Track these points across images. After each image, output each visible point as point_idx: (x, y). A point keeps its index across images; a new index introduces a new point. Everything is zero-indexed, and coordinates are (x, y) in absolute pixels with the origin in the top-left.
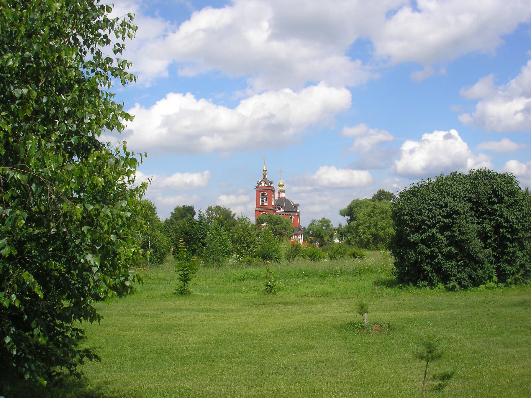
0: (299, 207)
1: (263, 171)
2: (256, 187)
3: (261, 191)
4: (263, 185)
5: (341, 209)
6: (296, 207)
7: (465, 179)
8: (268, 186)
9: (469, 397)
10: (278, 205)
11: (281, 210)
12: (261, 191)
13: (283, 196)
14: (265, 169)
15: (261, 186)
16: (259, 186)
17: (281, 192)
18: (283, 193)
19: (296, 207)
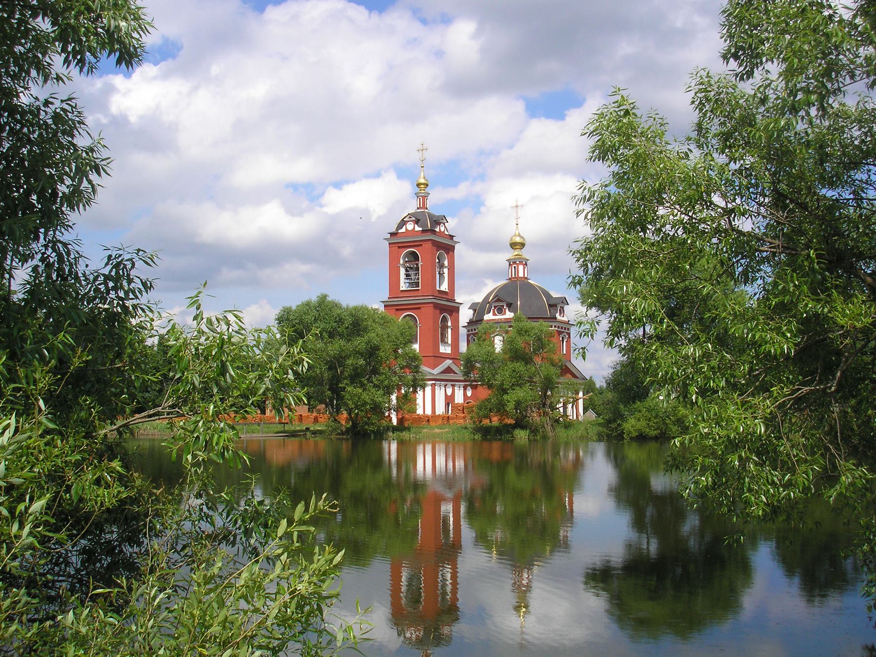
0: (566, 307)
1: (418, 185)
2: (392, 234)
3: (402, 246)
4: (410, 226)
5: (333, 296)
6: (555, 306)
7: (865, 305)
8: (423, 231)
9: (874, 247)
10: (499, 300)
11: (505, 314)
12: (402, 246)
13: (521, 275)
14: (422, 181)
15: (403, 230)
16: (400, 231)
17: (515, 263)
18: (521, 268)
19: (555, 306)
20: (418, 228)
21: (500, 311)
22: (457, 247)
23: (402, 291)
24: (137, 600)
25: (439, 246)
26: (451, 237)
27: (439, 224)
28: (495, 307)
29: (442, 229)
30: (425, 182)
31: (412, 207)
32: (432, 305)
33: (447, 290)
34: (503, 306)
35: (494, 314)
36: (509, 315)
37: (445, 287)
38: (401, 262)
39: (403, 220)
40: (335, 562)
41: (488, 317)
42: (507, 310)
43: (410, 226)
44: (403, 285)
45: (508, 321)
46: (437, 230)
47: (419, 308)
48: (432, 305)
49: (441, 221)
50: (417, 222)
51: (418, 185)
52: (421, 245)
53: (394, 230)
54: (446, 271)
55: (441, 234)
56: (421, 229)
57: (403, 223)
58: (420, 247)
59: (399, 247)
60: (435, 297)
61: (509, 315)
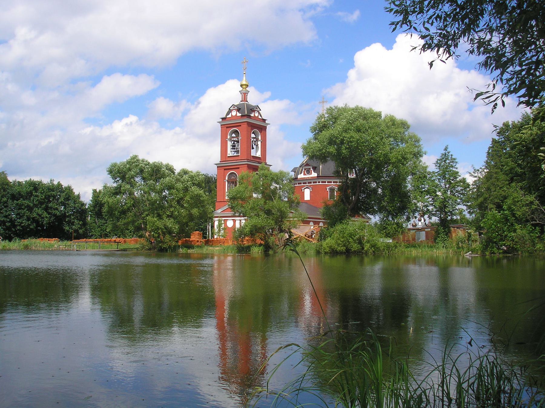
2: (223, 119)
3: (229, 127)
8: (242, 116)
12: (229, 127)
15: (230, 116)
16: (228, 117)
20: (239, 114)
21: (309, 172)
22: (268, 127)
23: (228, 157)
24: (152, 352)
25: (252, 126)
26: (264, 120)
27: (254, 111)
28: (305, 169)
29: (257, 115)
30: (247, 84)
31: (237, 100)
32: (246, 166)
33: (260, 156)
34: (310, 169)
35: (304, 174)
36: (314, 175)
37: (259, 154)
38: (229, 137)
39: (229, 109)
40: (495, 368)
41: (301, 176)
42: (313, 171)
43: (234, 113)
44: (230, 153)
45: (313, 178)
46: (252, 115)
47: (239, 168)
48: (246, 166)
49: (255, 109)
50: (239, 110)
51: (241, 86)
52: (240, 125)
53: (224, 116)
54: (259, 143)
55: (255, 118)
56: (241, 115)
57: (230, 111)
58: (240, 127)
59: (227, 127)
60: (248, 160)
61: (314, 175)
